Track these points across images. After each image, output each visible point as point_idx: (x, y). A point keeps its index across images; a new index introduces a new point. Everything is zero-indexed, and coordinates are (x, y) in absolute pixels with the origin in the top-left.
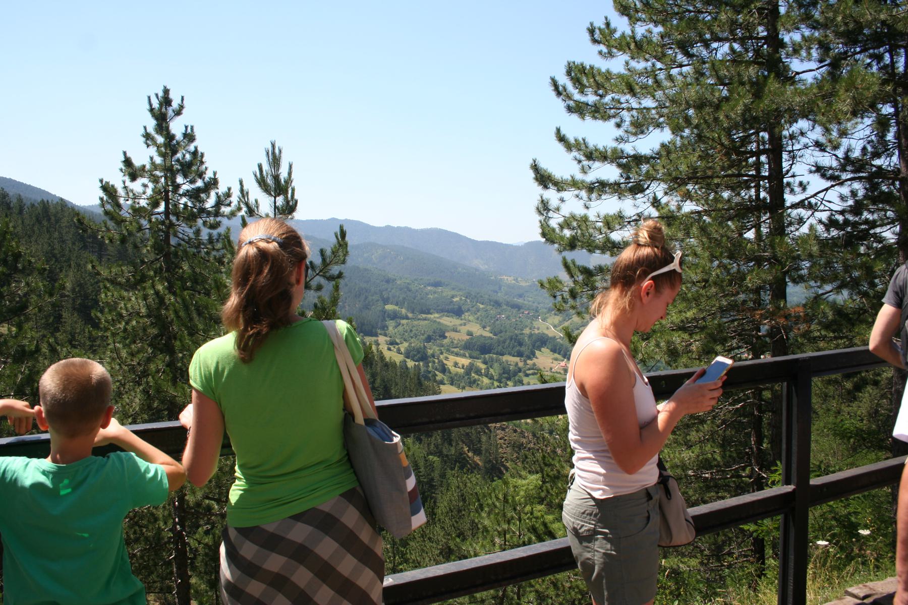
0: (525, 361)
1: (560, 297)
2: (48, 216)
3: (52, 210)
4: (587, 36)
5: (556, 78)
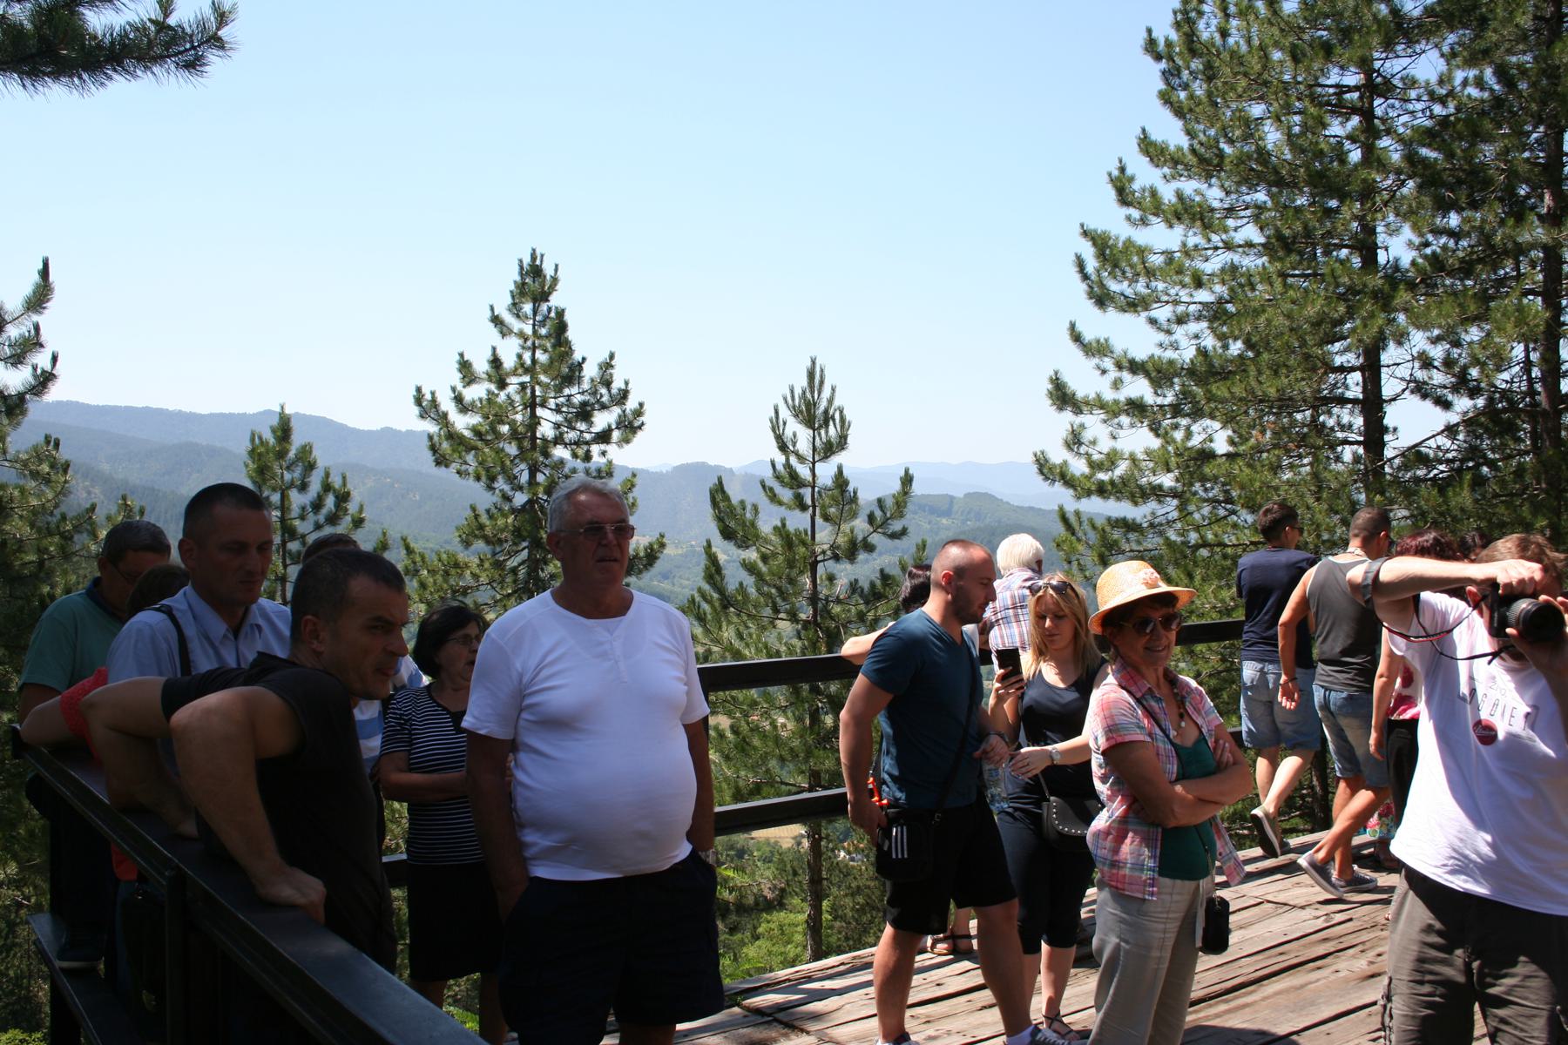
1: (1076, 563)
4: (1112, 194)
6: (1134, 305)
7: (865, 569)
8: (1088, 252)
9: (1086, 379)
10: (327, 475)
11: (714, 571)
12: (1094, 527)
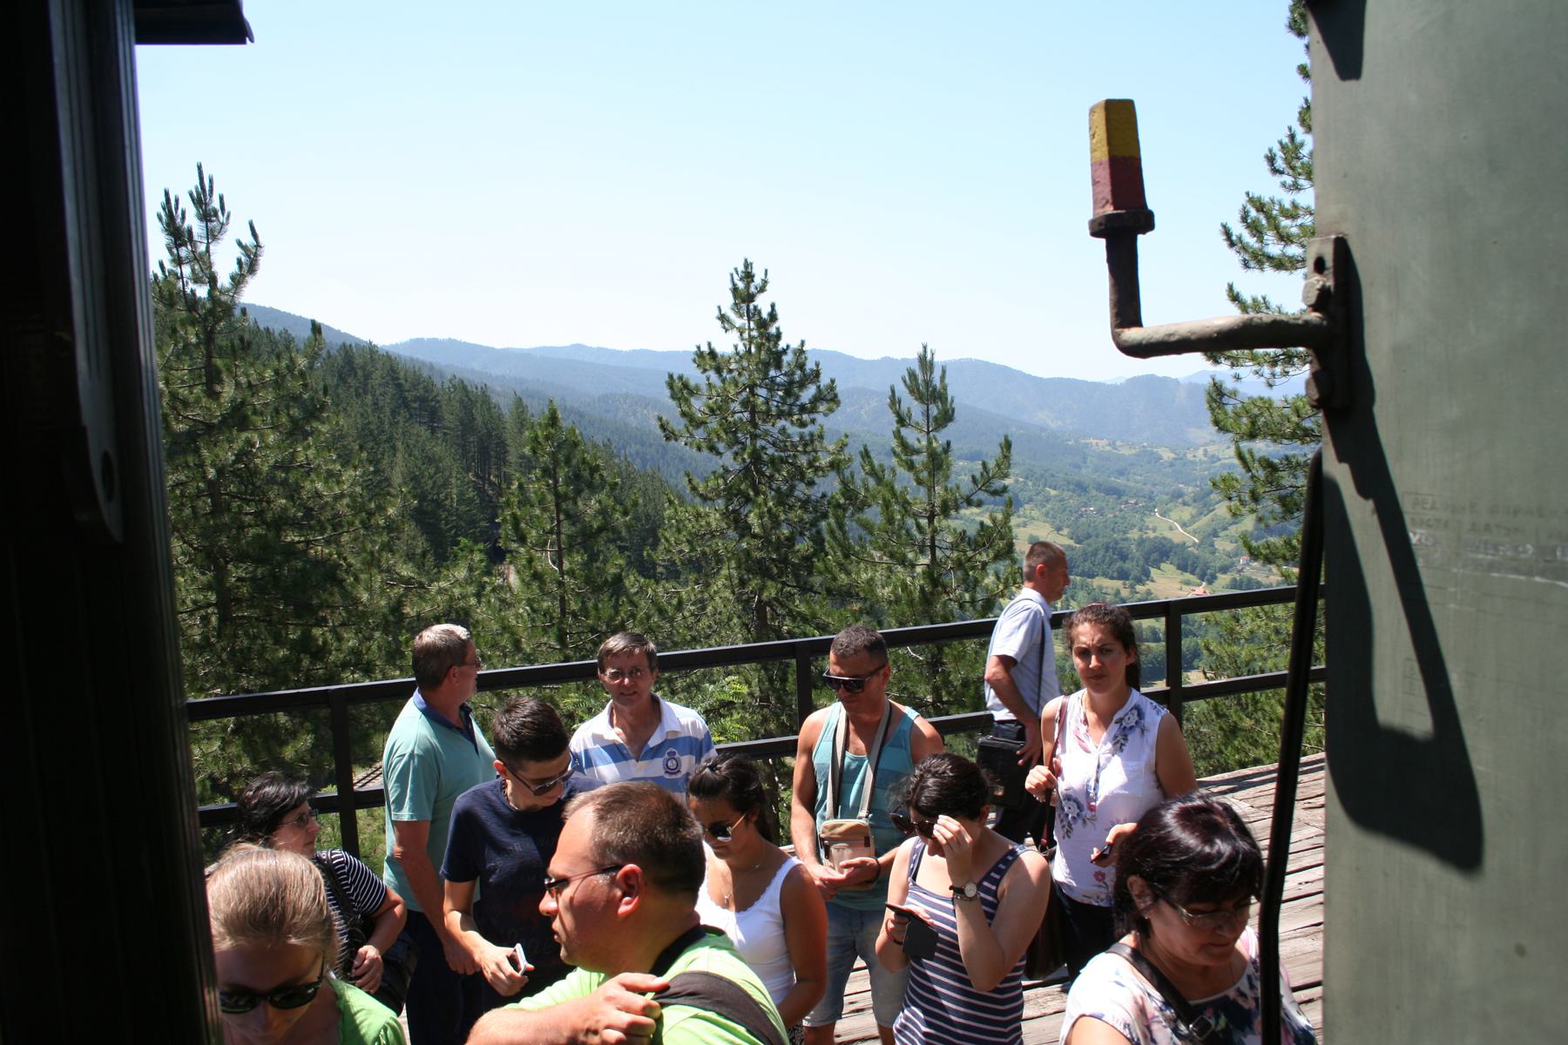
0: (1132, 587)
2: (353, 369)
3: (358, 361)
4: (1265, 166)
5: (1229, 225)
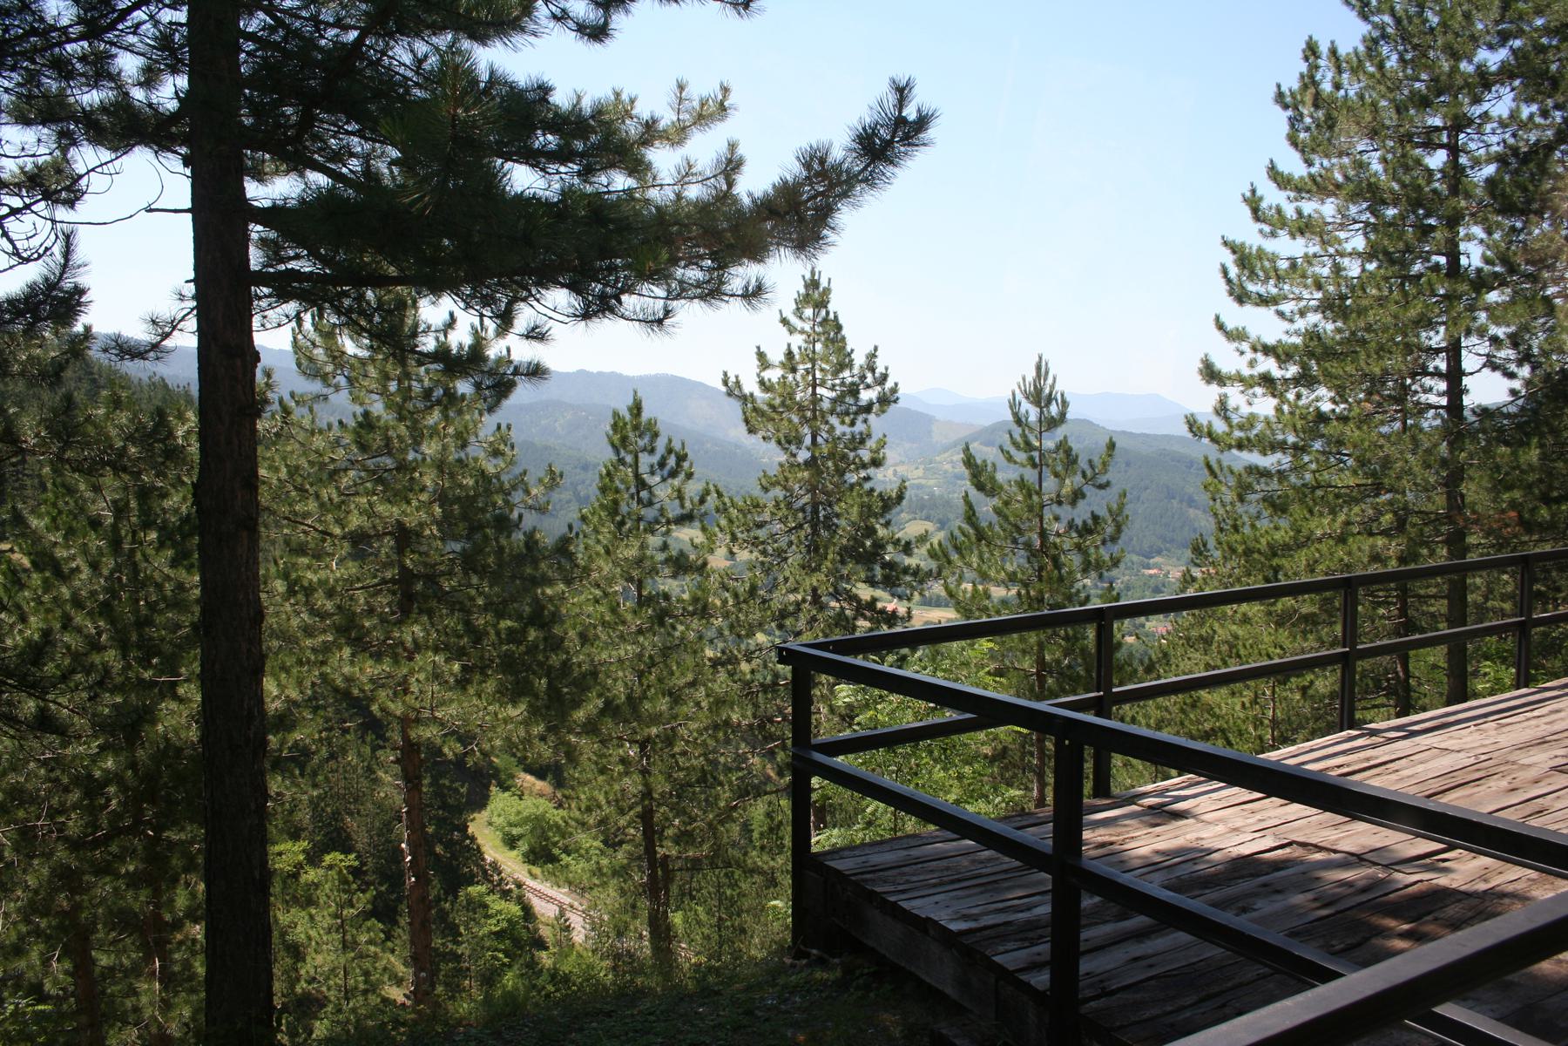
4: (1246, 211)
6: (1264, 301)
7: (1081, 513)
8: (1229, 259)
9: (1229, 359)
10: (670, 441)
11: (971, 515)
12: (1232, 472)
